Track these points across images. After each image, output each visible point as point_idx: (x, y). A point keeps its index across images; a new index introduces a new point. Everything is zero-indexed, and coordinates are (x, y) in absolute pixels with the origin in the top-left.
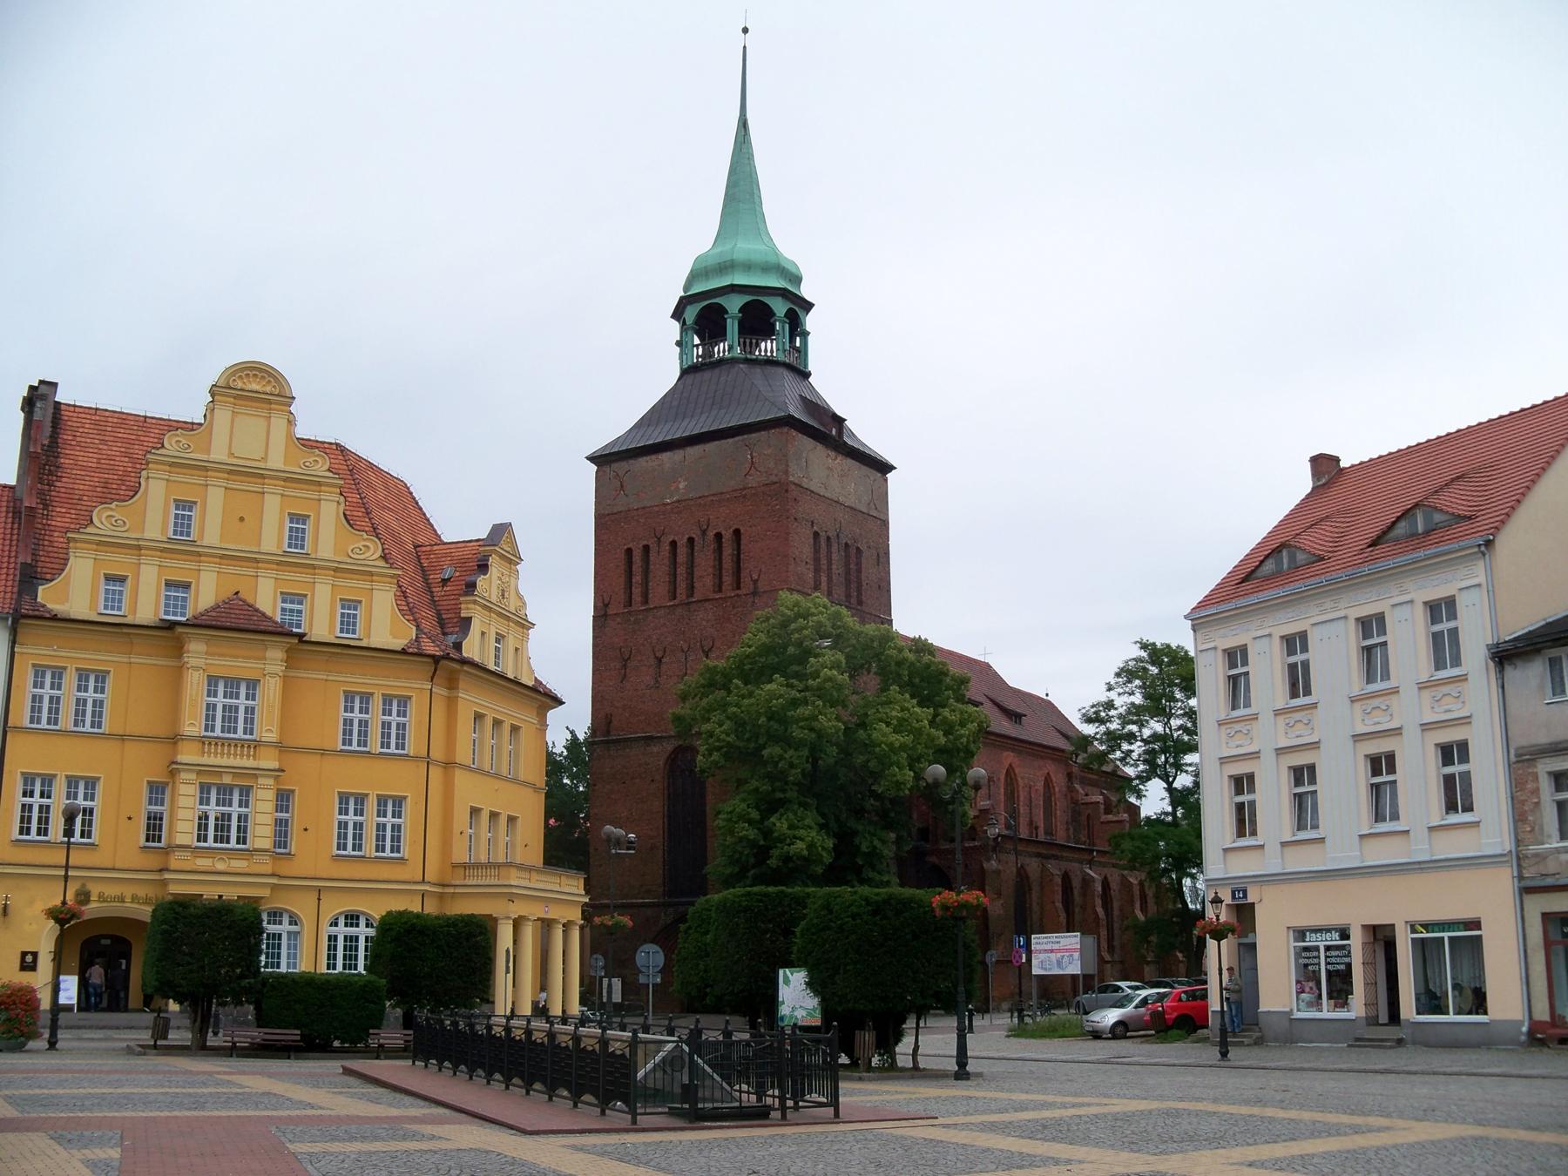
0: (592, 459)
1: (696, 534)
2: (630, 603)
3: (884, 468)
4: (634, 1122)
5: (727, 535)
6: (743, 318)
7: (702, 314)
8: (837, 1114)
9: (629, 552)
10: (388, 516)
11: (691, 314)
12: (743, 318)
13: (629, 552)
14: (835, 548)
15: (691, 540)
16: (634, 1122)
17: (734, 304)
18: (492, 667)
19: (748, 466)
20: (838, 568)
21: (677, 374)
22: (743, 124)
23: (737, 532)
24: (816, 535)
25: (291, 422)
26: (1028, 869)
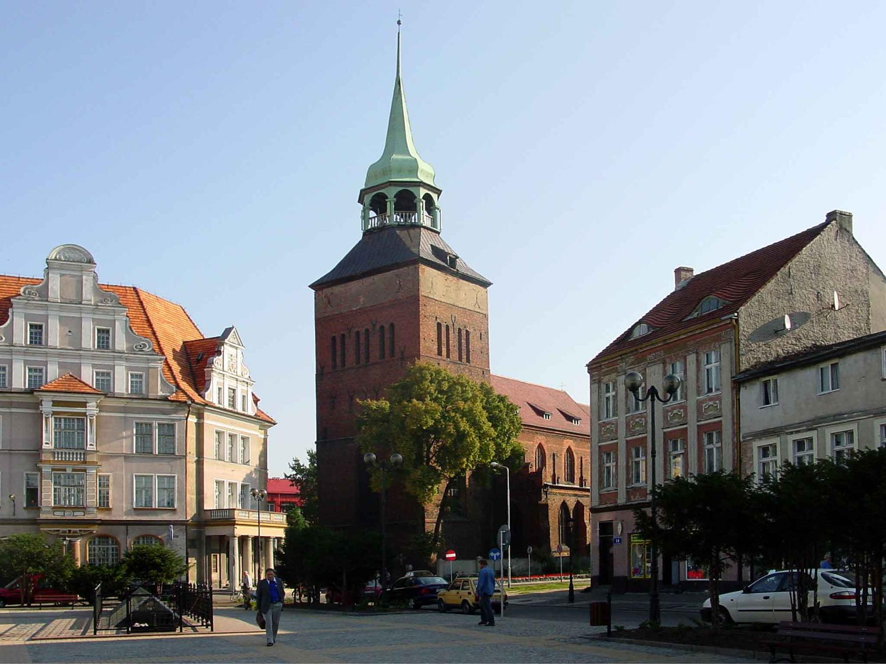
0: (311, 286)
1: (369, 327)
2: (358, 362)
3: (485, 284)
4: (95, 634)
5: (387, 326)
6: (395, 200)
7: (374, 199)
8: (212, 630)
9: (334, 339)
10: (166, 326)
11: (368, 199)
12: (395, 200)
13: (334, 339)
14: (451, 332)
15: (367, 330)
16: (95, 634)
17: (391, 193)
18: (217, 405)
19: (397, 287)
20: (453, 342)
21: (359, 237)
22: (398, 82)
23: (392, 325)
24: (439, 325)
25: (95, 278)
26: (568, 503)
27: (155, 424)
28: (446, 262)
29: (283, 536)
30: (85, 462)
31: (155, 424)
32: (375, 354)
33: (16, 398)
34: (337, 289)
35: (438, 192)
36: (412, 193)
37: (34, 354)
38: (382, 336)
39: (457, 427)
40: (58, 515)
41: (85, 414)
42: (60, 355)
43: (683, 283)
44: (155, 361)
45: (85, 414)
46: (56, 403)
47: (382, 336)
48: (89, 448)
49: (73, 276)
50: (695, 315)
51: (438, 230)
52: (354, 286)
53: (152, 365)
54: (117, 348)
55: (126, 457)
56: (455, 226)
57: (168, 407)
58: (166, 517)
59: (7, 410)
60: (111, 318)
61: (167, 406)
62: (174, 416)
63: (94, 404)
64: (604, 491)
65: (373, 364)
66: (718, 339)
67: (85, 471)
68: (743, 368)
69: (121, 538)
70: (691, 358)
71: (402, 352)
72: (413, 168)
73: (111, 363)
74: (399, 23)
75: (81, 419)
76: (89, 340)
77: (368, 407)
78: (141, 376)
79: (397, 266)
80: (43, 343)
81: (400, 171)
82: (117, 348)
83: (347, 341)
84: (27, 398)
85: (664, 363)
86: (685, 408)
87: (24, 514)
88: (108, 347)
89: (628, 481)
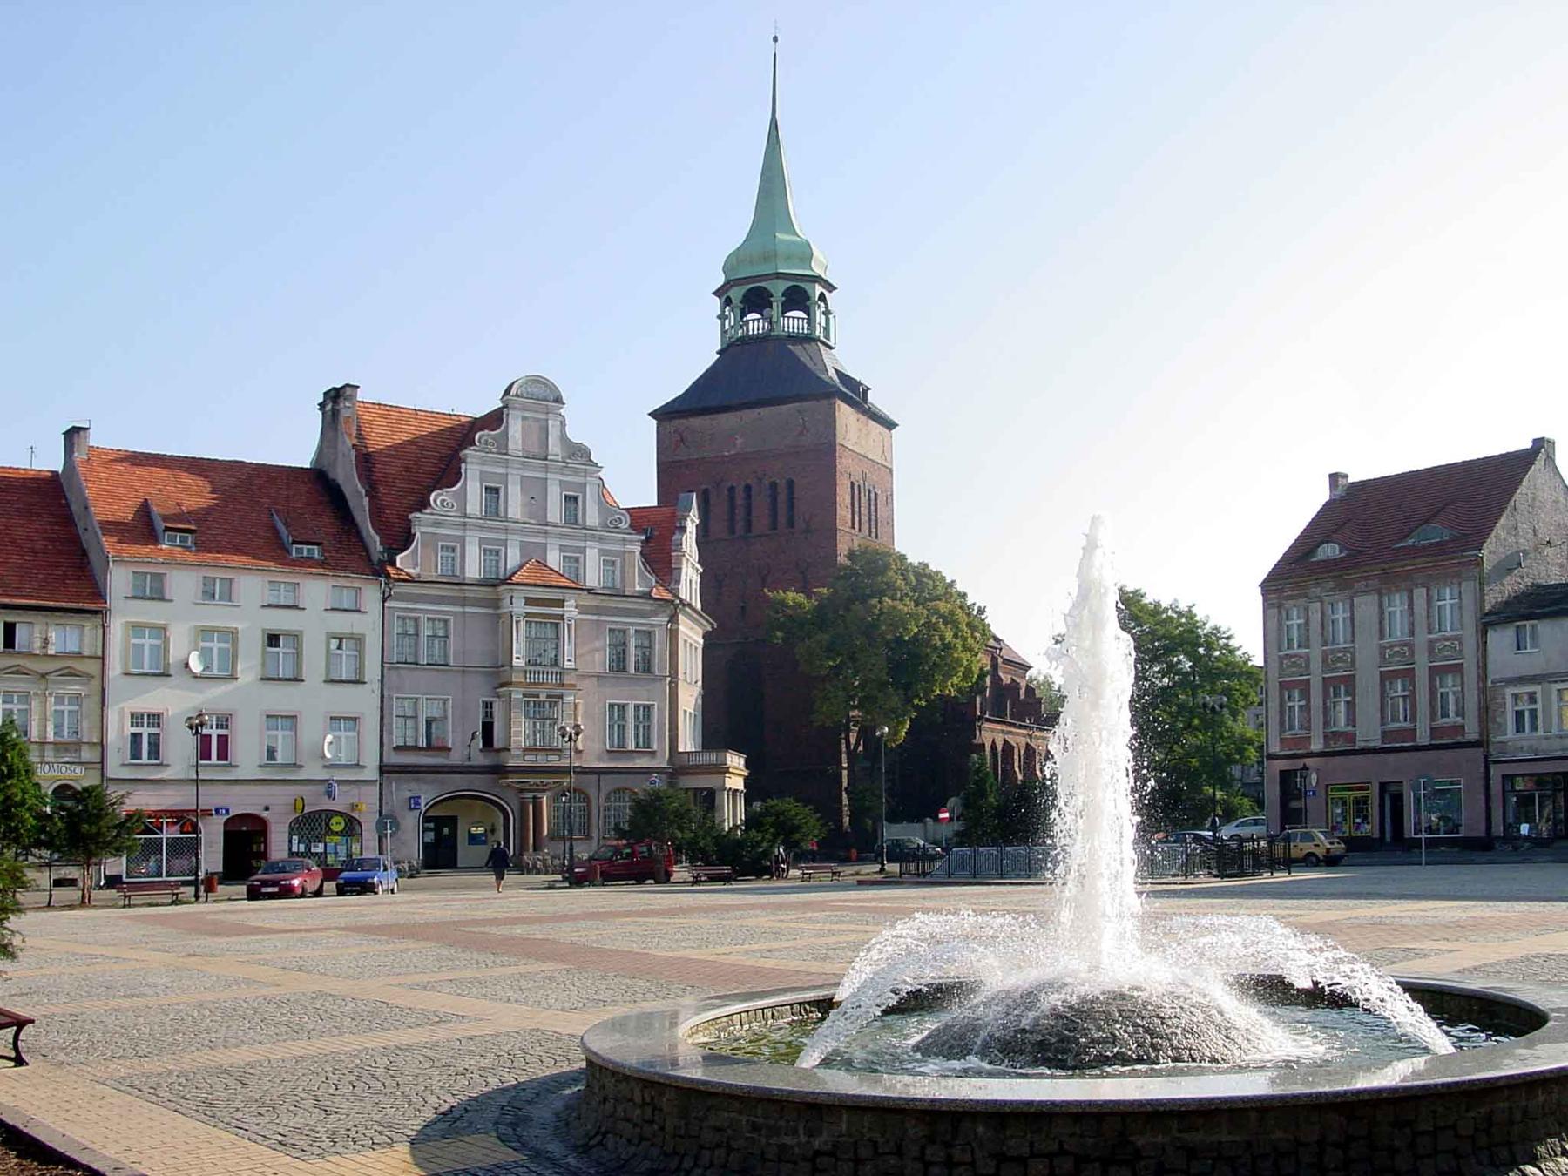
2: (732, 531)
3: (890, 425)
5: (782, 484)
6: (770, 292)
12: (770, 292)
17: (778, 289)
22: (774, 125)
28: (855, 394)
32: (761, 521)
33: (471, 592)
34: (696, 422)
35: (831, 288)
37: (491, 529)
39: (942, 638)
40: (530, 760)
41: (562, 617)
43: (1339, 491)
44: (631, 541)
45: (562, 617)
46: (529, 601)
50: (1410, 542)
52: (727, 420)
54: (589, 523)
55: (599, 677)
56: (851, 343)
57: (648, 608)
58: (642, 762)
60: (581, 480)
61: (647, 606)
62: (654, 620)
63: (572, 602)
66: (1458, 575)
68: (1488, 607)
69: (592, 793)
70: (1420, 593)
72: (805, 254)
73: (581, 544)
74: (775, 39)
75: (557, 622)
76: (555, 512)
77: (783, 603)
78: (613, 563)
79: (798, 398)
81: (788, 258)
82: (589, 523)
85: (1381, 595)
86: (1410, 646)
88: (576, 523)
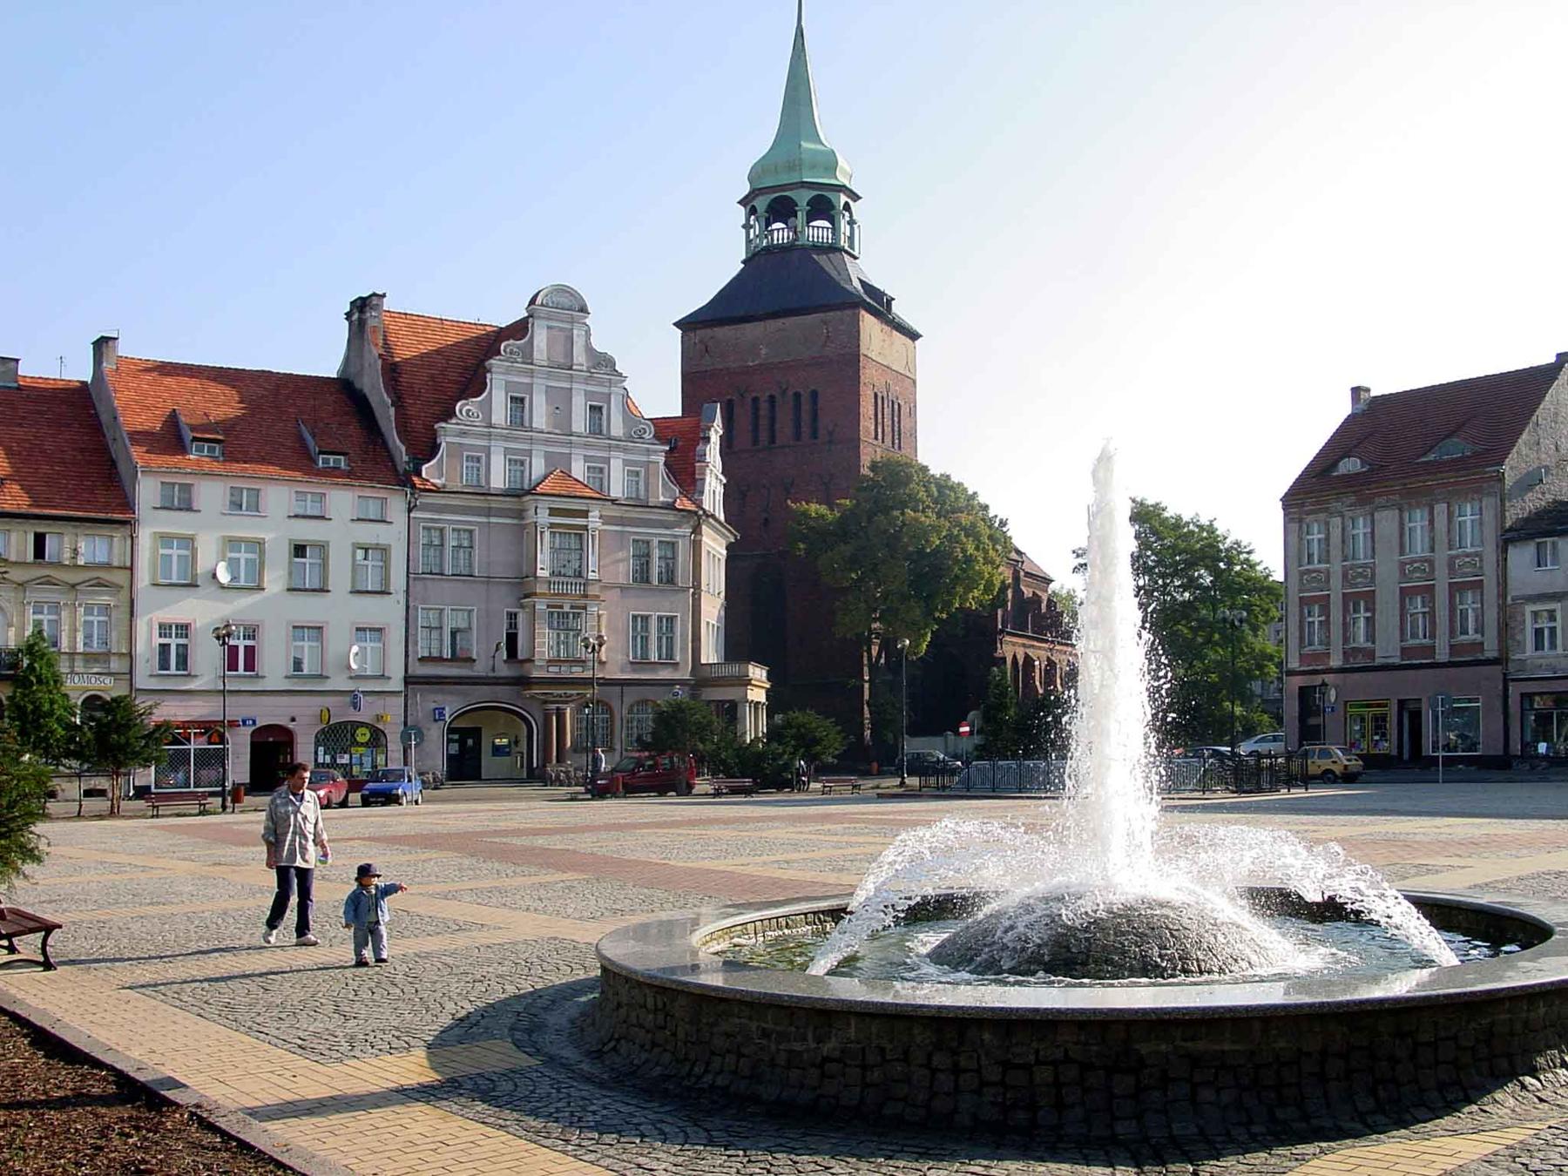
2: (755, 441)
3: (914, 336)
6: (795, 200)
12: (795, 200)
15: (772, 397)
17: (803, 198)
23: (814, 394)
27: (655, 541)
28: (879, 304)
29: (763, 700)
30: (586, 596)
31: (655, 541)
33: (496, 503)
35: (856, 197)
36: (829, 201)
37: (516, 439)
38: (798, 407)
39: (964, 551)
41: (586, 528)
42: (547, 442)
43: (1362, 406)
44: (655, 452)
45: (586, 528)
46: (553, 512)
47: (798, 407)
48: (591, 576)
49: (561, 329)
50: (1431, 457)
51: (856, 253)
52: (752, 331)
53: (653, 458)
54: (613, 433)
55: (623, 588)
59: (484, 520)
60: (606, 390)
61: (670, 517)
62: (677, 531)
63: (597, 513)
64: (1306, 650)
65: (783, 447)
66: (1478, 491)
67: (585, 608)
69: (616, 705)
71: (831, 433)
72: (831, 164)
73: (605, 454)
76: (580, 423)
77: (805, 514)
80: (527, 424)
82: (613, 433)
83: (737, 410)
84: (509, 503)
87: (504, 671)
89: (1346, 640)
